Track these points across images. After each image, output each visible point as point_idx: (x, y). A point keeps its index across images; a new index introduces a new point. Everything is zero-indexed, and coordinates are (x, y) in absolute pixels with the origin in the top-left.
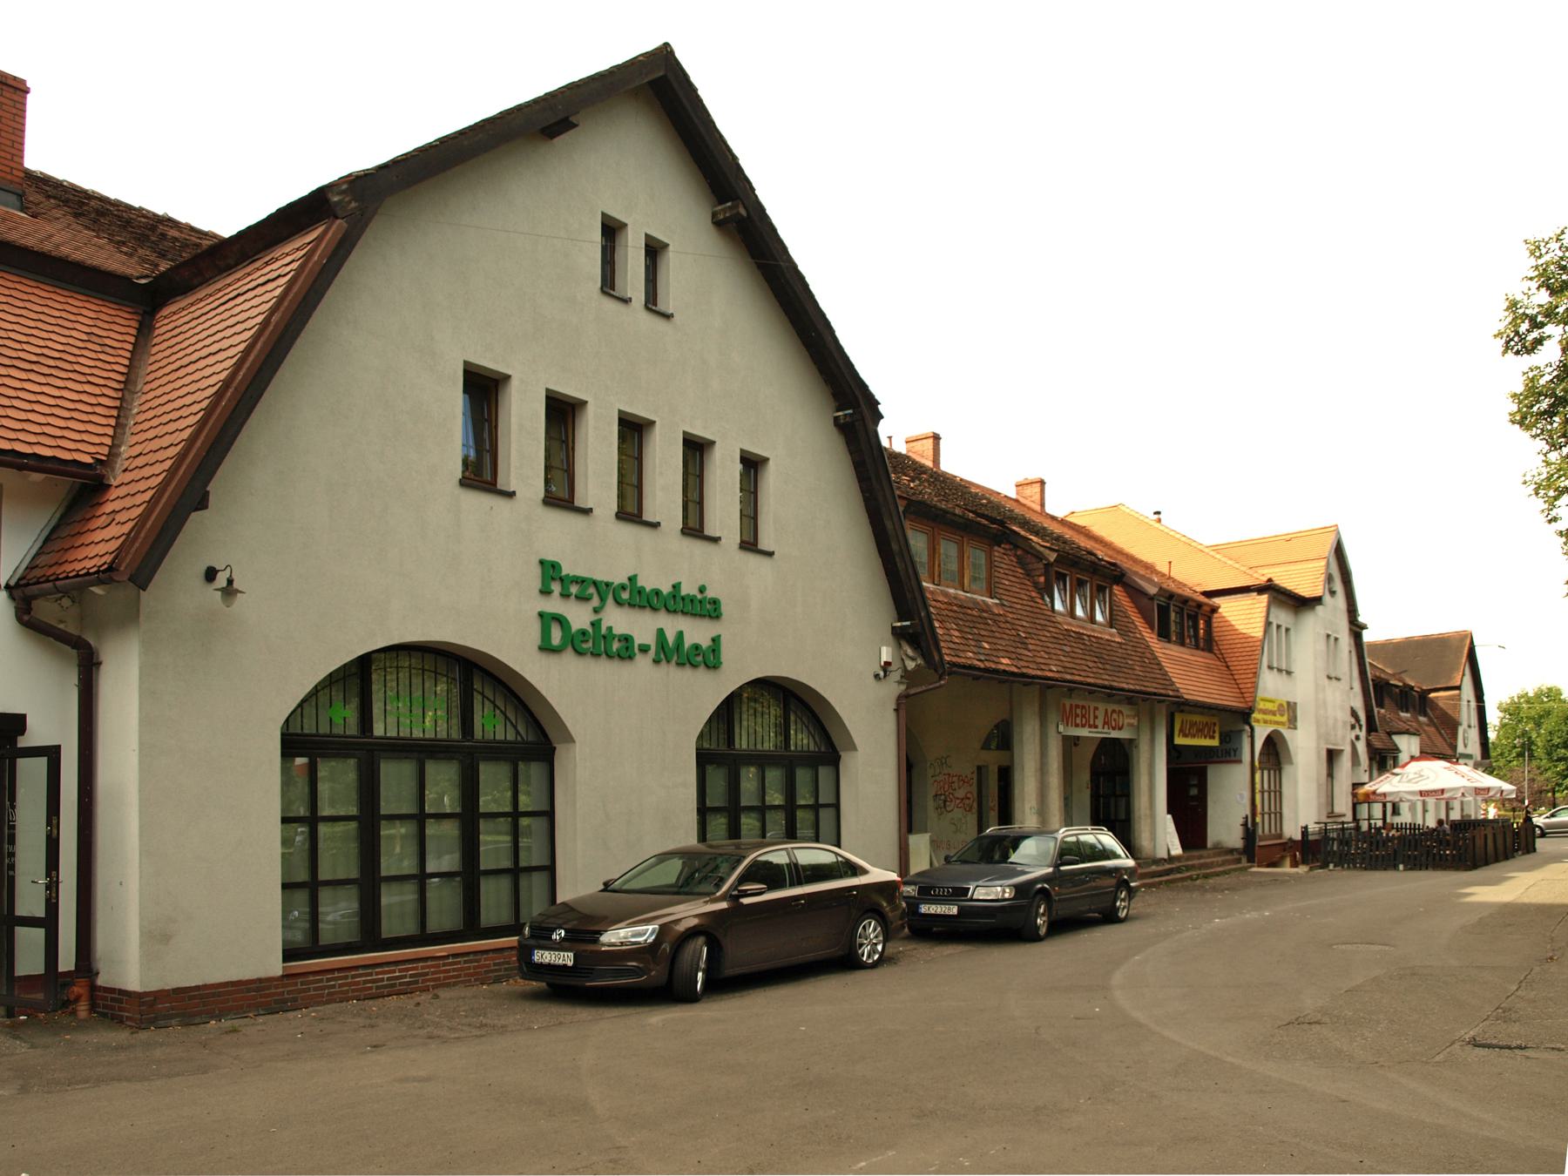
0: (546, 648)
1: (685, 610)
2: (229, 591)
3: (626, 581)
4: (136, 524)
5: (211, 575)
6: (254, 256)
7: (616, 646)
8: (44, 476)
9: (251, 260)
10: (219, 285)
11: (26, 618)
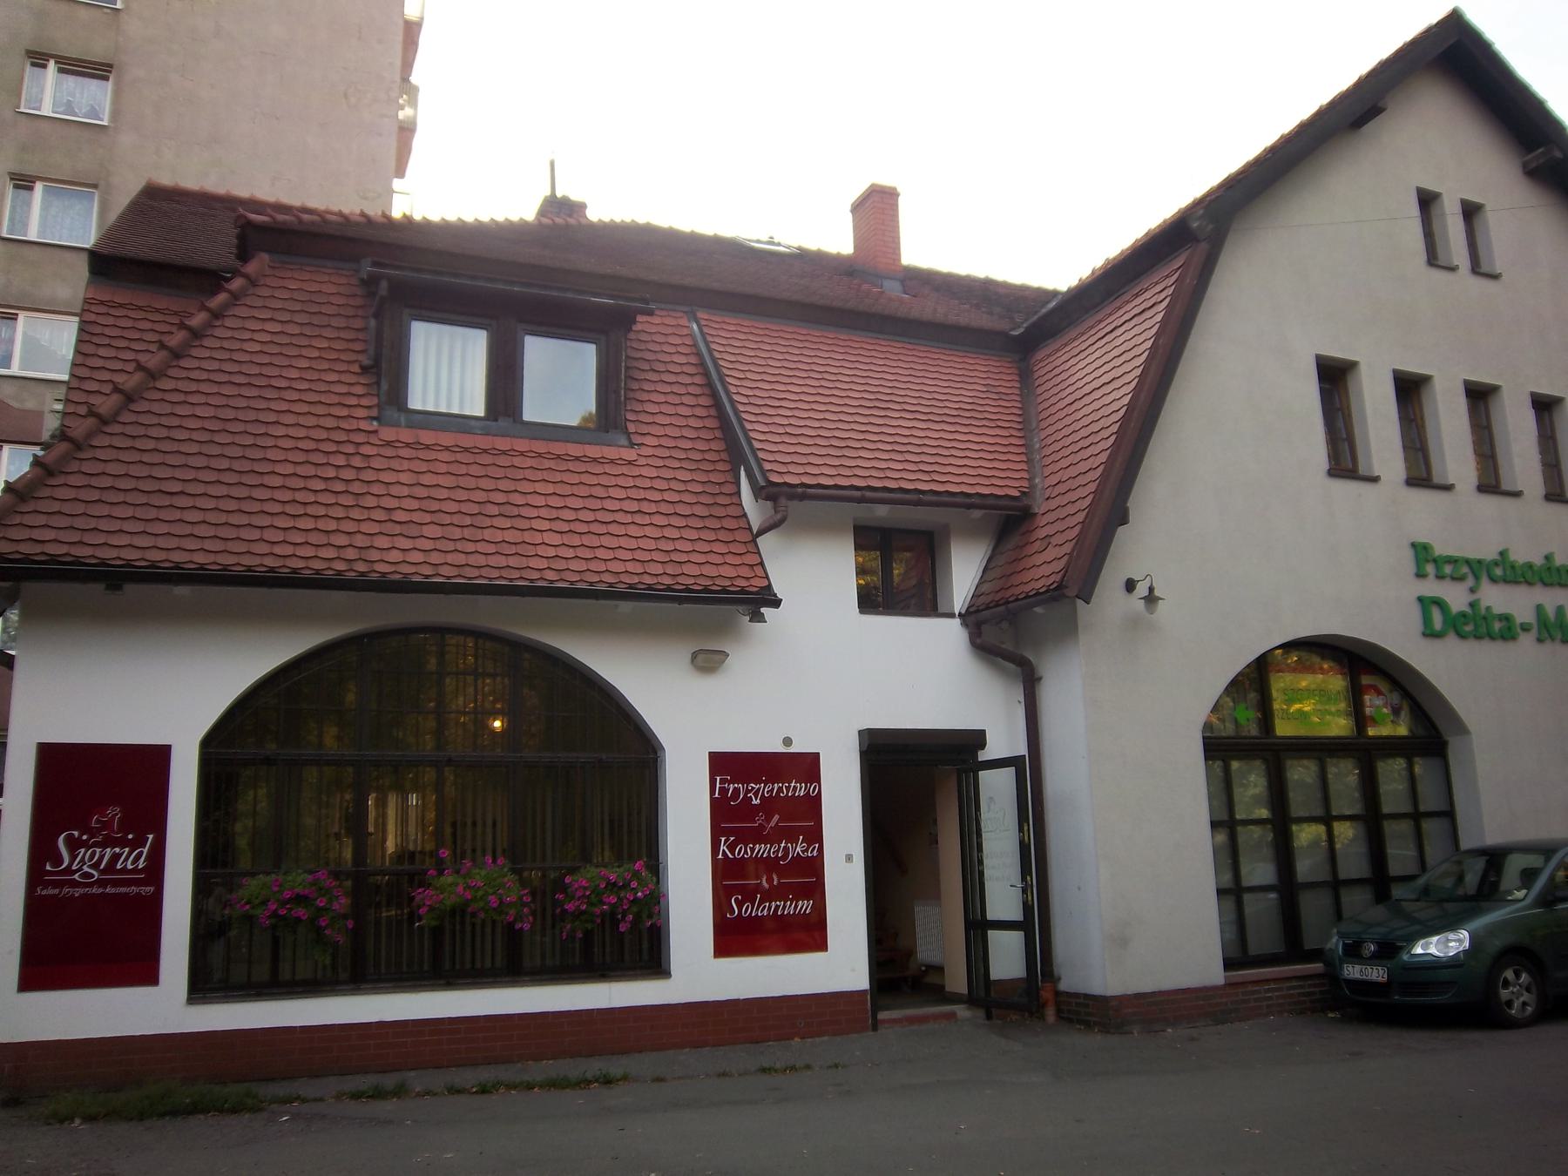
0: (1430, 634)
1: (1563, 582)
2: (1151, 599)
3: (1498, 557)
4: (1076, 544)
5: (1130, 586)
6: (1119, 290)
7: (1497, 626)
8: (983, 511)
9: (1116, 295)
10: (1091, 322)
11: (978, 641)
